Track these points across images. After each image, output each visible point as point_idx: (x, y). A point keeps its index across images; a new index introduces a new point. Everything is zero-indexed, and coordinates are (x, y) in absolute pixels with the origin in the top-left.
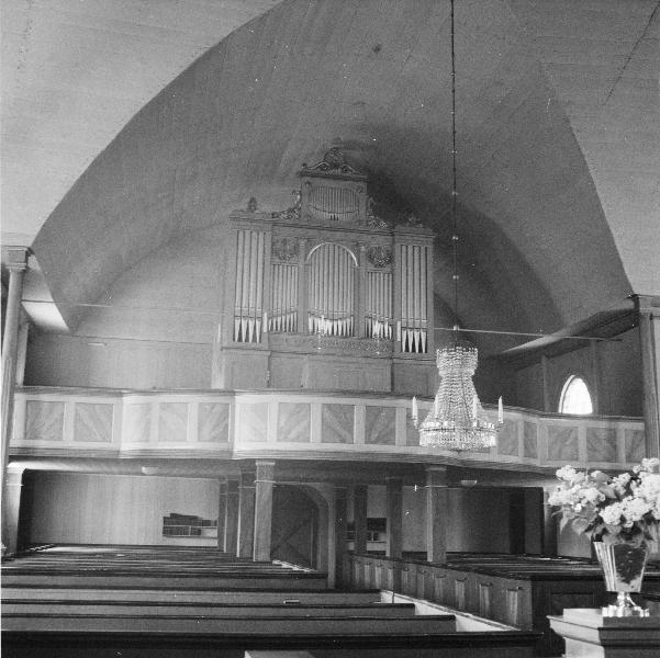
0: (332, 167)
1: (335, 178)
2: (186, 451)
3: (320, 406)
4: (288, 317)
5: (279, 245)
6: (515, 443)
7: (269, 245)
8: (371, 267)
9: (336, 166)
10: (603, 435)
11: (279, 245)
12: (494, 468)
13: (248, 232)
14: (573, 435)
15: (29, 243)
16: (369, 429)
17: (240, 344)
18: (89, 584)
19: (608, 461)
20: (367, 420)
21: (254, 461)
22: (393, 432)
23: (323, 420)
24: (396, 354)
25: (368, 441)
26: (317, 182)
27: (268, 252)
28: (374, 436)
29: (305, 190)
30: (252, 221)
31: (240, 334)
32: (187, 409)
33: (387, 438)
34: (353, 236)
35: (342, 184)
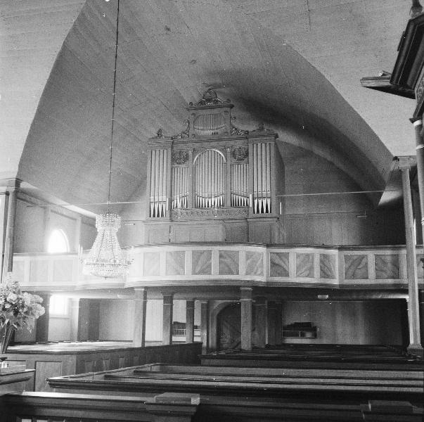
0: (207, 102)
1: (211, 108)
2: (310, 284)
3: (165, 254)
4: (213, 199)
5: (177, 156)
6: (311, 268)
7: (170, 157)
8: (234, 161)
9: (209, 100)
10: (389, 259)
11: (177, 156)
12: (306, 286)
13: (259, 144)
14: (364, 261)
15: (14, 175)
16: (195, 263)
17: (258, 215)
18: (291, 374)
19: (393, 278)
20: (193, 258)
21: (239, 287)
22: (210, 266)
23: (167, 261)
24: (251, 214)
25: (194, 273)
26: (201, 112)
27: (169, 161)
28: (198, 269)
29: (192, 119)
30: (264, 136)
31: (158, 214)
32: (107, 265)
33: (206, 270)
34: (221, 143)
35: (216, 111)
